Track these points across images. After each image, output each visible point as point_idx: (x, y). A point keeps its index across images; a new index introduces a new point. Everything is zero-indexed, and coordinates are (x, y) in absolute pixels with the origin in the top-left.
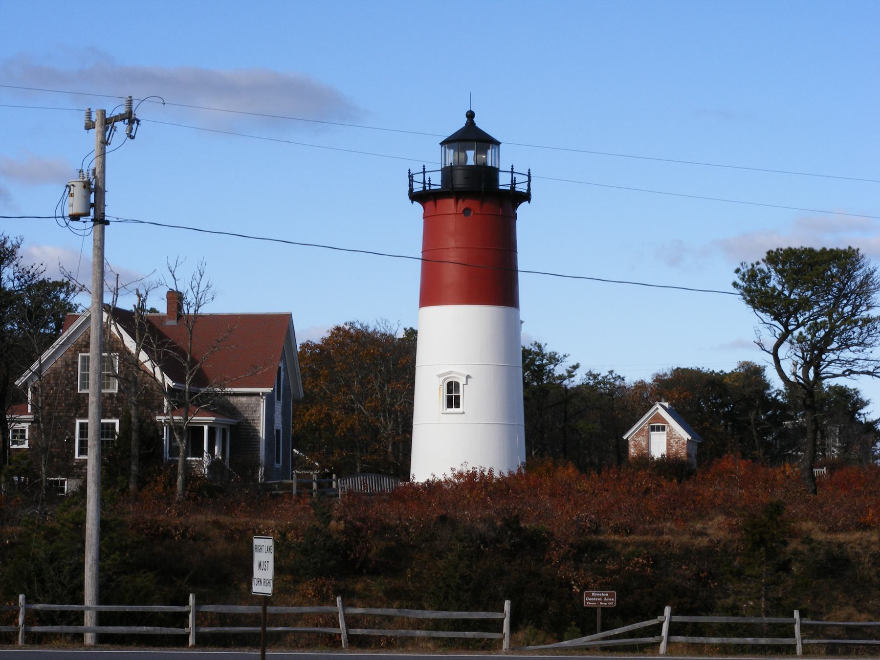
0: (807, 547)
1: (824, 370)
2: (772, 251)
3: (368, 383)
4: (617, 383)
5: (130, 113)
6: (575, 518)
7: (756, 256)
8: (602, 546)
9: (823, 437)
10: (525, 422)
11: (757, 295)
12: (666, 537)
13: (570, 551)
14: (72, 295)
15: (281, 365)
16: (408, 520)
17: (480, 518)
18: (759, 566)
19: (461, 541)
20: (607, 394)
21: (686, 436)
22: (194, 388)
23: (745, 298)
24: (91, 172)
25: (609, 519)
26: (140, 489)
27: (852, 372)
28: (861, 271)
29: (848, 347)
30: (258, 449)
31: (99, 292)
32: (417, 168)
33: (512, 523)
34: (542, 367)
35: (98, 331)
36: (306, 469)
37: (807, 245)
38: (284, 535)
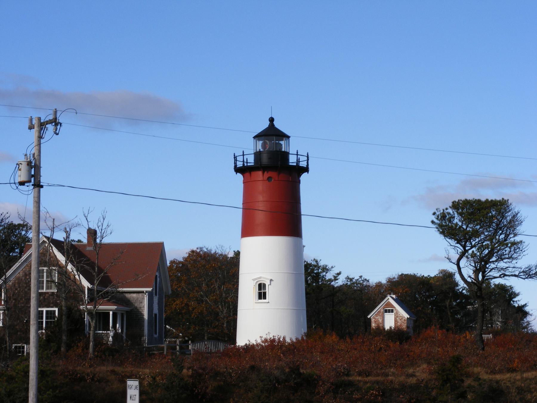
0: (477, 383)
1: (488, 274)
2: (455, 202)
3: (212, 285)
4: (365, 283)
5: (56, 118)
6: (334, 366)
7: (445, 205)
8: (351, 384)
9: (491, 315)
10: (307, 307)
11: (447, 228)
12: (390, 378)
13: (331, 387)
14: (30, 232)
15: (157, 274)
16: (231, 368)
17: (276, 367)
18: (446, 395)
19: (262, 381)
20: (359, 290)
21: (406, 316)
22: (100, 288)
23: (439, 230)
24: (32, 155)
25: (356, 367)
26: (67, 351)
27: (505, 275)
28: (510, 213)
29: (502, 260)
30: (143, 326)
31: (37, 229)
32: (239, 153)
33: (295, 370)
34: (318, 274)
35: (37, 253)
36: (174, 338)
37: (477, 198)
38: (154, 379)
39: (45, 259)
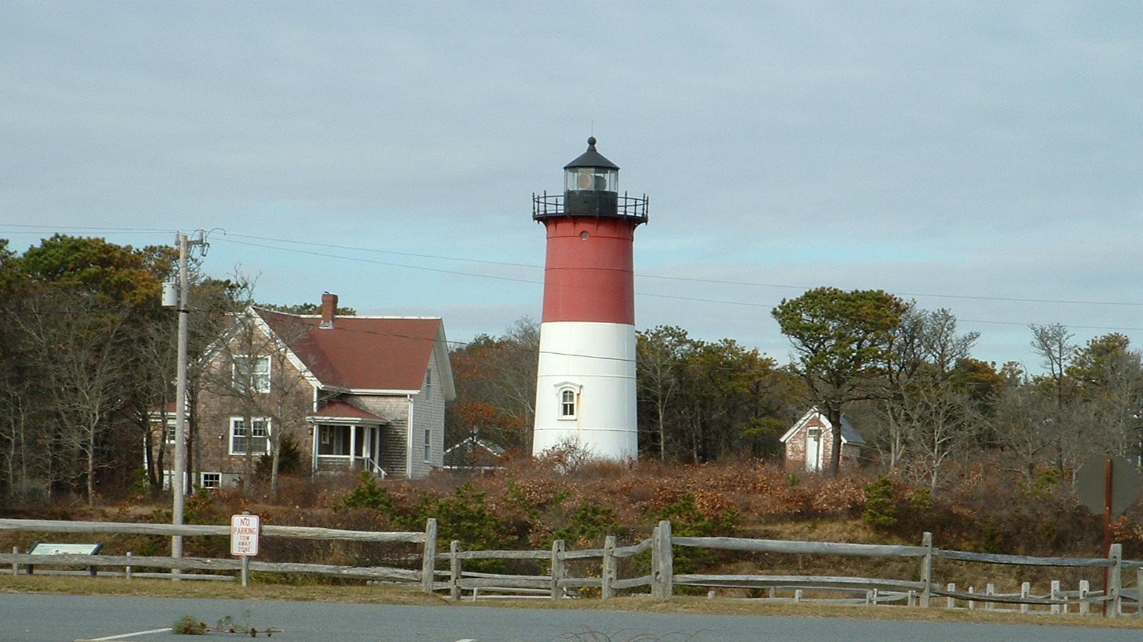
11: (788, 316)
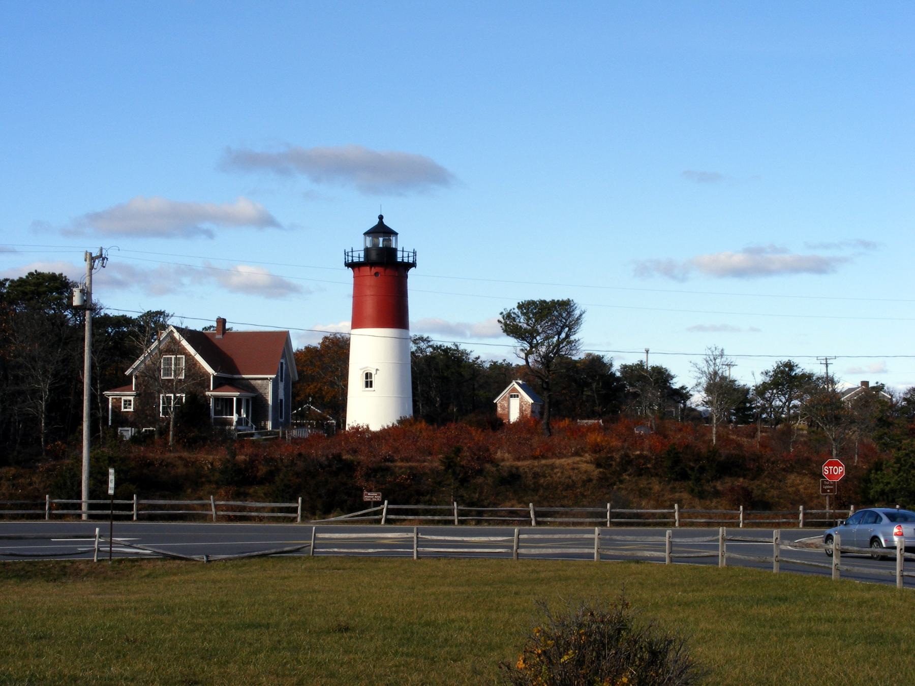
7: (512, 305)
11: (511, 328)
21: (531, 401)
30: (268, 411)
39: (174, 348)
